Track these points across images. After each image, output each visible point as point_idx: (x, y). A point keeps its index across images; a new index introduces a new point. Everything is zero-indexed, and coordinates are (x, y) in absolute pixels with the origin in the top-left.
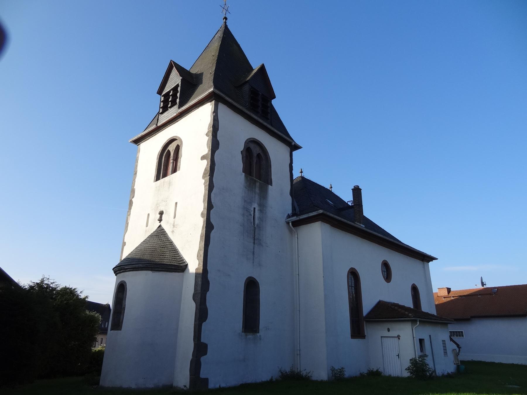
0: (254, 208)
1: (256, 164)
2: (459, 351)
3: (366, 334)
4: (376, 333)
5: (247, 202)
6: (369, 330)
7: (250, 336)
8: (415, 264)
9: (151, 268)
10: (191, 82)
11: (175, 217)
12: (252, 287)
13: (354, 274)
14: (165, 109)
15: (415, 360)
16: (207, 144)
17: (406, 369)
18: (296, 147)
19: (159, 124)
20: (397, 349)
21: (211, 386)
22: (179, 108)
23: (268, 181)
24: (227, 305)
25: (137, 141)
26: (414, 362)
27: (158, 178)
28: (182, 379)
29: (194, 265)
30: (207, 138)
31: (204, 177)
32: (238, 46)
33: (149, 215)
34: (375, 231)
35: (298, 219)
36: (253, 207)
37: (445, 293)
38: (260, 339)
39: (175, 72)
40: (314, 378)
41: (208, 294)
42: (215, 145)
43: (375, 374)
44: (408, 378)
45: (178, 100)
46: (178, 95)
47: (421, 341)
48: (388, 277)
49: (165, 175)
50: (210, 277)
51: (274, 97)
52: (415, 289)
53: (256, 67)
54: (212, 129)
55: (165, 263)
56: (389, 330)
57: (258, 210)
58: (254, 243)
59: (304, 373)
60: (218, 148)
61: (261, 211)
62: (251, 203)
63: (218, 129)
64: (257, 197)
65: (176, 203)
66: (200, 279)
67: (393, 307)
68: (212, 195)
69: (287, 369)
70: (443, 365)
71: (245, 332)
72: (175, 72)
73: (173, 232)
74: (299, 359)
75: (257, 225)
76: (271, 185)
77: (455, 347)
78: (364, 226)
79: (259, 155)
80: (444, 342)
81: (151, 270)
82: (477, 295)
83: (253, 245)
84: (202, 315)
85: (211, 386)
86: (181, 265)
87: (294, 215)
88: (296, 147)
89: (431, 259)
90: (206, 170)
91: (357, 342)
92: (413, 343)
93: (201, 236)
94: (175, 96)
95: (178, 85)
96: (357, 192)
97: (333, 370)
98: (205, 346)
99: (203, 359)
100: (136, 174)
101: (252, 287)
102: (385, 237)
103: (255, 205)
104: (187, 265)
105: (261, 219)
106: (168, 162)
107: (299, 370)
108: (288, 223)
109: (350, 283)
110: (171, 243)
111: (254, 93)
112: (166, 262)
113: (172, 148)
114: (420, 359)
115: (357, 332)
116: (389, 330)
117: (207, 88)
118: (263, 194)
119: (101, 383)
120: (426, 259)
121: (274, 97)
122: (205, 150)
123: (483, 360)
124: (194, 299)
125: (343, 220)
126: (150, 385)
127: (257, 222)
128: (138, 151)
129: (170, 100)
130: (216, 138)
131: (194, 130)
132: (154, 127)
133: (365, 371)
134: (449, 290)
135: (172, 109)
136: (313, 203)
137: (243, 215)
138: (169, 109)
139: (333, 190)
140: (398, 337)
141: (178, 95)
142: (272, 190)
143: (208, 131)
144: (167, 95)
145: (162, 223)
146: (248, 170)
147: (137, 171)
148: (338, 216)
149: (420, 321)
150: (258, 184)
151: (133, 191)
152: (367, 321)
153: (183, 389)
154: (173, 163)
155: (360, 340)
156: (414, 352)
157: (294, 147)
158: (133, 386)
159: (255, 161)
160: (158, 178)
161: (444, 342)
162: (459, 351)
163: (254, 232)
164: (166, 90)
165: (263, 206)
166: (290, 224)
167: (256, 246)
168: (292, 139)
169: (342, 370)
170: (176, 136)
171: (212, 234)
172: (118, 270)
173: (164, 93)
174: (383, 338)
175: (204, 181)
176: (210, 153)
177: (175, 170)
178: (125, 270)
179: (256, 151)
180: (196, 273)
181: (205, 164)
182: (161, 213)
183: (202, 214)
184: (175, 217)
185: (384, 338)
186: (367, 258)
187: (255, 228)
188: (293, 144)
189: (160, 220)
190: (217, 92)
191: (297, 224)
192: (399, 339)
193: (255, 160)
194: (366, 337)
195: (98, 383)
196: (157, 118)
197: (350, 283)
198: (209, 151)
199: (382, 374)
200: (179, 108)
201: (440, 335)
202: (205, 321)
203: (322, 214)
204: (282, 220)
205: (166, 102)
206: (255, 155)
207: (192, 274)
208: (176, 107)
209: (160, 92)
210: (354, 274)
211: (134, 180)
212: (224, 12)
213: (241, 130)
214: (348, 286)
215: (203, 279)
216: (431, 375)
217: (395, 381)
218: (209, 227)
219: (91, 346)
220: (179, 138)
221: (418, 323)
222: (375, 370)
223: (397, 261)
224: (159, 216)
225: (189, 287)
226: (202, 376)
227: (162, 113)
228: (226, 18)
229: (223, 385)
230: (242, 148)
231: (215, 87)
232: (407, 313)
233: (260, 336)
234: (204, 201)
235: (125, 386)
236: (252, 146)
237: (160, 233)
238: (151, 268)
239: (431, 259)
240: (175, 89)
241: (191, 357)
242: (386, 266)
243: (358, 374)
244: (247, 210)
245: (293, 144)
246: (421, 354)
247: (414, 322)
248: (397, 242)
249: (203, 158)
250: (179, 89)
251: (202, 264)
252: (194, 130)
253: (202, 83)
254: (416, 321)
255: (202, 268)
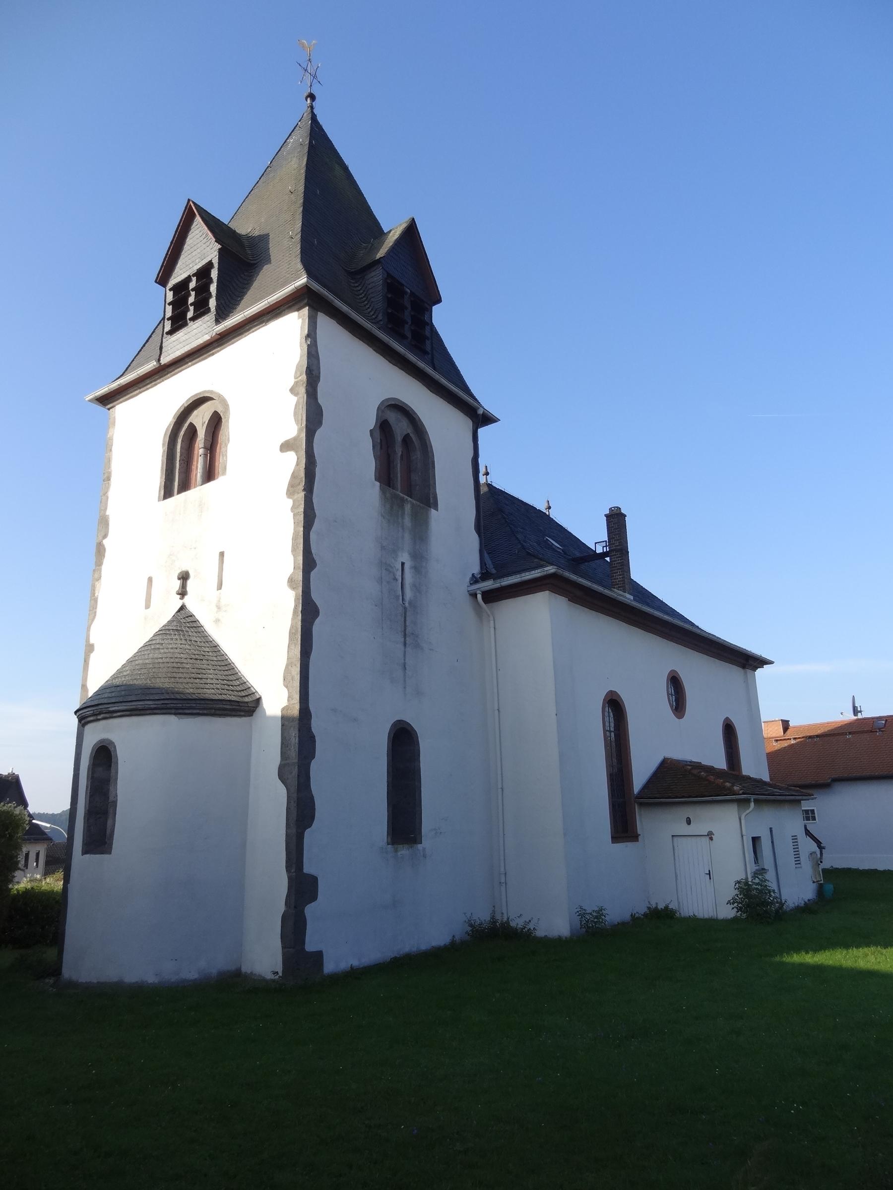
0: (403, 564)
1: (402, 460)
2: (821, 854)
3: (639, 832)
4: (659, 827)
5: (389, 549)
6: (647, 822)
7: (404, 851)
8: (733, 672)
9: (176, 709)
10: (241, 258)
11: (220, 587)
12: (403, 740)
13: (614, 705)
14: (178, 322)
15: (746, 883)
16: (295, 414)
17: (729, 903)
18: (487, 419)
19: (165, 360)
20: (705, 863)
21: (330, 966)
22: (218, 321)
23: (428, 500)
24: (353, 783)
25: (107, 400)
26: (744, 888)
27: (168, 493)
28: (265, 957)
29: (276, 698)
30: (293, 400)
31: (290, 493)
32: (345, 169)
33: (150, 580)
34: (648, 605)
35: (497, 585)
36: (401, 560)
37: (779, 731)
38: (425, 856)
39: (199, 227)
40: (540, 933)
41: (314, 765)
42: (314, 417)
43: (662, 916)
44: (735, 920)
45: (213, 303)
46: (213, 288)
47: (755, 840)
48: (679, 705)
49: (185, 486)
50: (316, 726)
51: (439, 300)
52: (729, 730)
53: (393, 226)
54: (304, 377)
55: (207, 696)
56: (689, 822)
57: (411, 568)
58: (405, 644)
59: (517, 923)
60: (320, 423)
61: (417, 569)
62: (394, 552)
63: (318, 378)
64: (407, 536)
65: (222, 554)
66: (294, 735)
67: (695, 772)
68: (313, 536)
69: (482, 915)
70: (796, 888)
71: (393, 844)
72: (199, 227)
73: (217, 621)
74: (504, 893)
75: (410, 603)
76: (436, 507)
77: (814, 847)
78: (632, 598)
79: (406, 440)
80: (795, 838)
81: (175, 714)
82: (839, 734)
83: (402, 647)
84: (302, 812)
85: (330, 966)
86: (246, 699)
87: (485, 575)
88: (487, 419)
89: (761, 662)
90: (294, 476)
91: (624, 849)
92: (741, 846)
93: (292, 634)
94: (203, 291)
95: (210, 265)
96: (616, 521)
97: (582, 914)
98: (313, 881)
99: (310, 910)
100: (109, 479)
101: (403, 740)
102: (666, 617)
103: (404, 557)
104: (258, 701)
105: (417, 588)
106: (192, 452)
107: (505, 919)
108: (474, 595)
109: (607, 724)
110: (215, 648)
111: (393, 287)
112: (210, 693)
113: (200, 419)
114: (757, 881)
115: (624, 829)
116: (689, 822)
117: (286, 273)
118: (420, 531)
119: (68, 972)
120: (749, 662)
121: (439, 300)
122: (291, 427)
123: (854, 866)
124: (281, 776)
125: (595, 587)
126: (190, 973)
127: (409, 594)
128: (108, 424)
129: (191, 299)
130: (316, 399)
131: (261, 374)
132: (152, 365)
133: (641, 909)
134: (786, 725)
135: (199, 322)
136: (522, 549)
137: (380, 580)
138: (191, 324)
139: (554, 515)
140: (710, 836)
141: (213, 288)
142: (437, 518)
143: (296, 383)
144: (181, 288)
145: (187, 600)
146: (385, 476)
147: (110, 473)
148: (575, 573)
149: (756, 801)
150: (408, 508)
151: (104, 522)
152: (641, 805)
153: (273, 981)
154: (205, 455)
155: (629, 844)
156: (743, 867)
157: (481, 419)
158: (151, 979)
159: (400, 454)
160: (168, 493)
161: (795, 838)
162: (821, 854)
163: (403, 619)
164: (177, 277)
165: (419, 558)
166: (479, 596)
167: (409, 649)
168: (476, 399)
169: (600, 913)
170: (211, 392)
171: (317, 627)
172: (89, 713)
173: (174, 280)
174: (675, 839)
175: (290, 502)
176: (303, 435)
177: (210, 475)
178: (111, 715)
179: (401, 428)
180: (283, 718)
181: (290, 463)
182: (184, 577)
183: (291, 581)
184: (220, 587)
185: (680, 839)
186: (635, 664)
187: (405, 608)
188: (480, 412)
189: (183, 593)
190: (315, 286)
191: (491, 597)
192: (711, 839)
193: (399, 450)
194: (640, 838)
195: (56, 970)
196: (153, 342)
197: (607, 724)
198: (300, 431)
199: (677, 915)
200: (218, 321)
201: (787, 824)
202: (310, 826)
203: (553, 576)
204: (462, 587)
205: (179, 304)
206: (399, 438)
207: (274, 718)
208: (209, 318)
209: (162, 279)
210: (614, 705)
211: (105, 494)
212: (308, 79)
213: (371, 380)
214: (605, 731)
215: (301, 732)
216: (777, 911)
217: (705, 928)
218: (309, 611)
219: (11, 881)
220: (220, 396)
221: (752, 804)
222: (661, 906)
223: (696, 670)
224: (178, 584)
225: (267, 749)
226: (310, 946)
227: (171, 333)
228: (312, 97)
229: (355, 963)
230: (371, 422)
231: (310, 274)
232: (728, 784)
233: (424, 849)
234: (294, 550)
235: (131, 978)
236: (393, 417)
237: (184, 624)
238: (176, 709)
239: (761, 662)
240: (203, 273)
241: (282, 908)
242: (675, 681)
243: (627, 917)
244: (386, 567)
245: (480, 412)
246: (755, 868)
247: (743, 803)
248: (694, 630)
249: (286, 447)
250: (214, 274)
251: (297, 697)
252: (261, 374)
253: (268, 260)
254: (748, 801)
255: (297, 707)
